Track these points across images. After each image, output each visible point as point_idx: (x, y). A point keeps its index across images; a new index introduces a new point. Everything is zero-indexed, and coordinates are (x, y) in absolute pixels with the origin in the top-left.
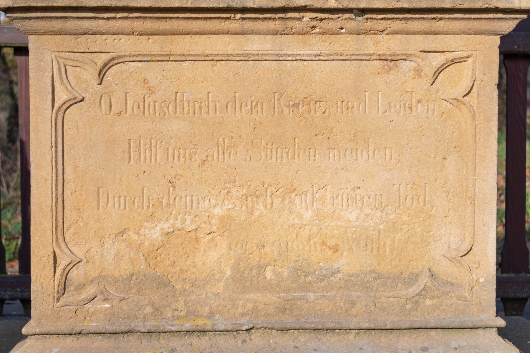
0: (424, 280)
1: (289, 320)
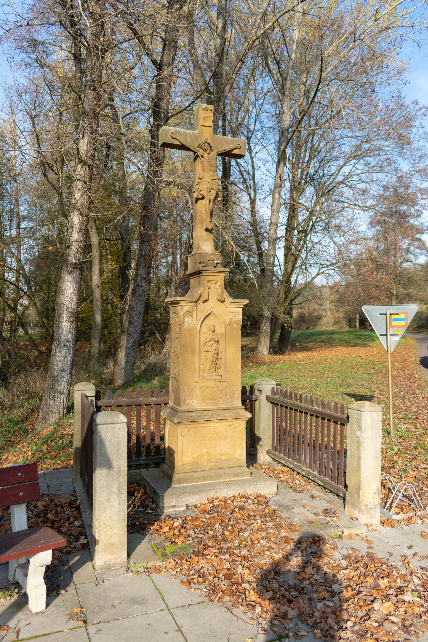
0: (235, 459)
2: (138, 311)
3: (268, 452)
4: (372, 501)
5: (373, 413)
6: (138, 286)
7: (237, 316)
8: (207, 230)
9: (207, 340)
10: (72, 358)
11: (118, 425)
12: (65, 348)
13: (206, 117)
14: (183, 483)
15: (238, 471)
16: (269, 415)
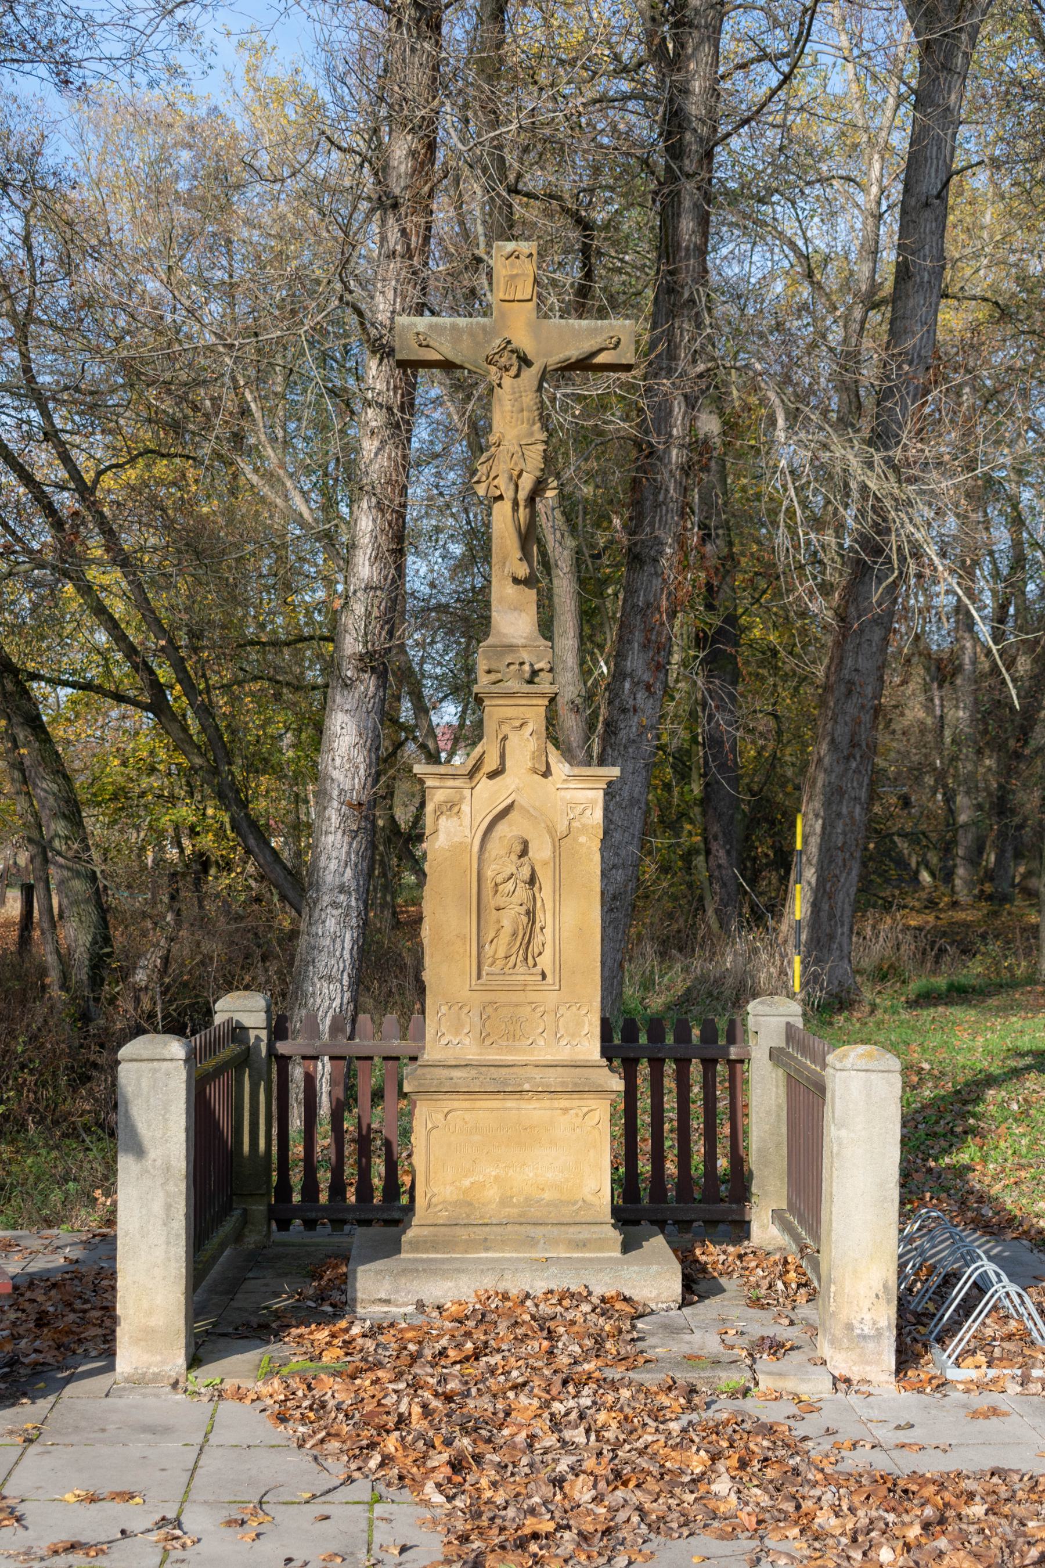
0: (580, 1203)
1: (523, 1220)
2: (626, 794)
3: (778, 1216)
4: (867, 1317)
5: (873, 1076)
6: (624, 711)
7: (588, 812)
8: (516, 581)
9: (499, 879)
10: (355, 942)
11: (165, 1064)
12: (336, 912)
13: (513, 277)
14: (427, 1252)
15: (585, 1233)
16: (779, 1106)
